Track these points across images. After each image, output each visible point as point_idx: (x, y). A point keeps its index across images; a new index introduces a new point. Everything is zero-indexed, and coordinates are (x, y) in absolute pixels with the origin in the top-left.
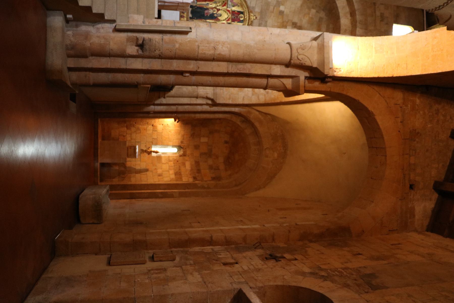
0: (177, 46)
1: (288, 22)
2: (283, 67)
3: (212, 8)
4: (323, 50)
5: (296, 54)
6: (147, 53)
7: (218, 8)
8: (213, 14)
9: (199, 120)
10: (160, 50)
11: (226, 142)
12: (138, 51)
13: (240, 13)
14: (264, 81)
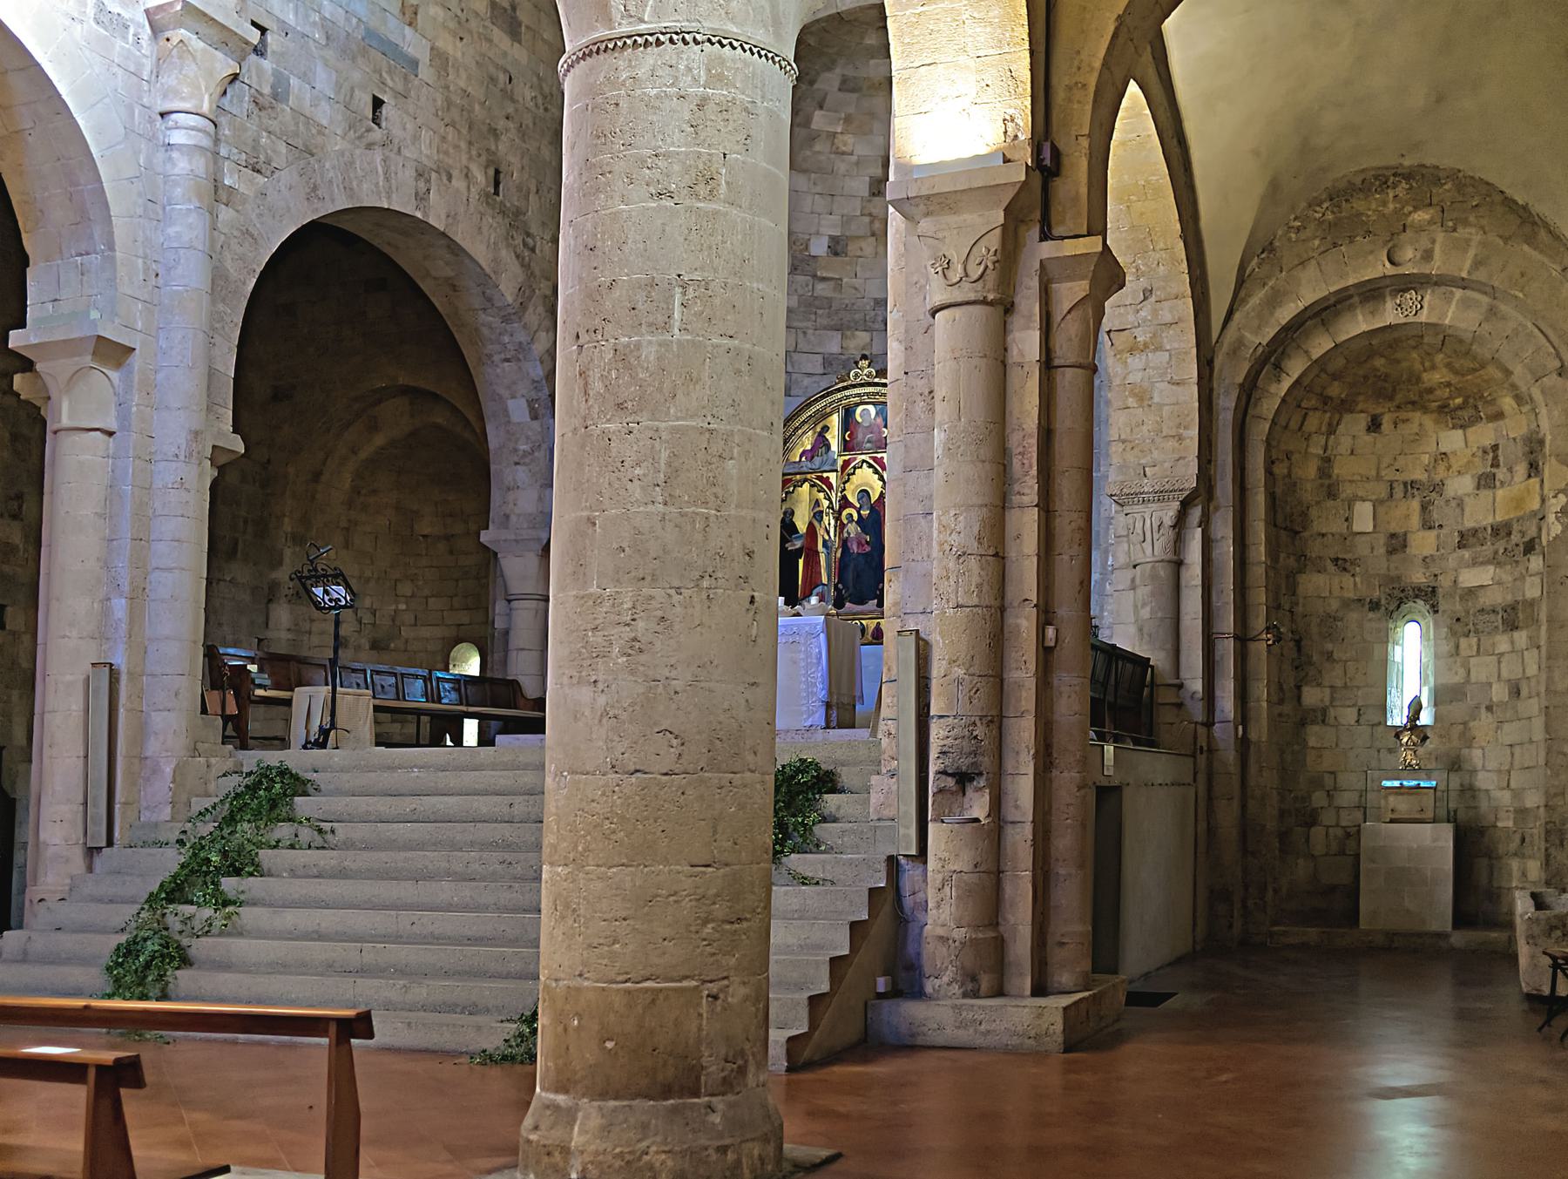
0: (960, 672)
1: (870, 215)
2: (1016, 321)
3: (841, 527)
4: (939, 197)
5: (966, 285)
6: (986, 762)
7: (836, 507)
8: (861, 521)
9: (1273, 550)
10: (974, 724)
11: (1375, 425)
12: (979, 789)
13: (848, 422)
14: (1068, 380)
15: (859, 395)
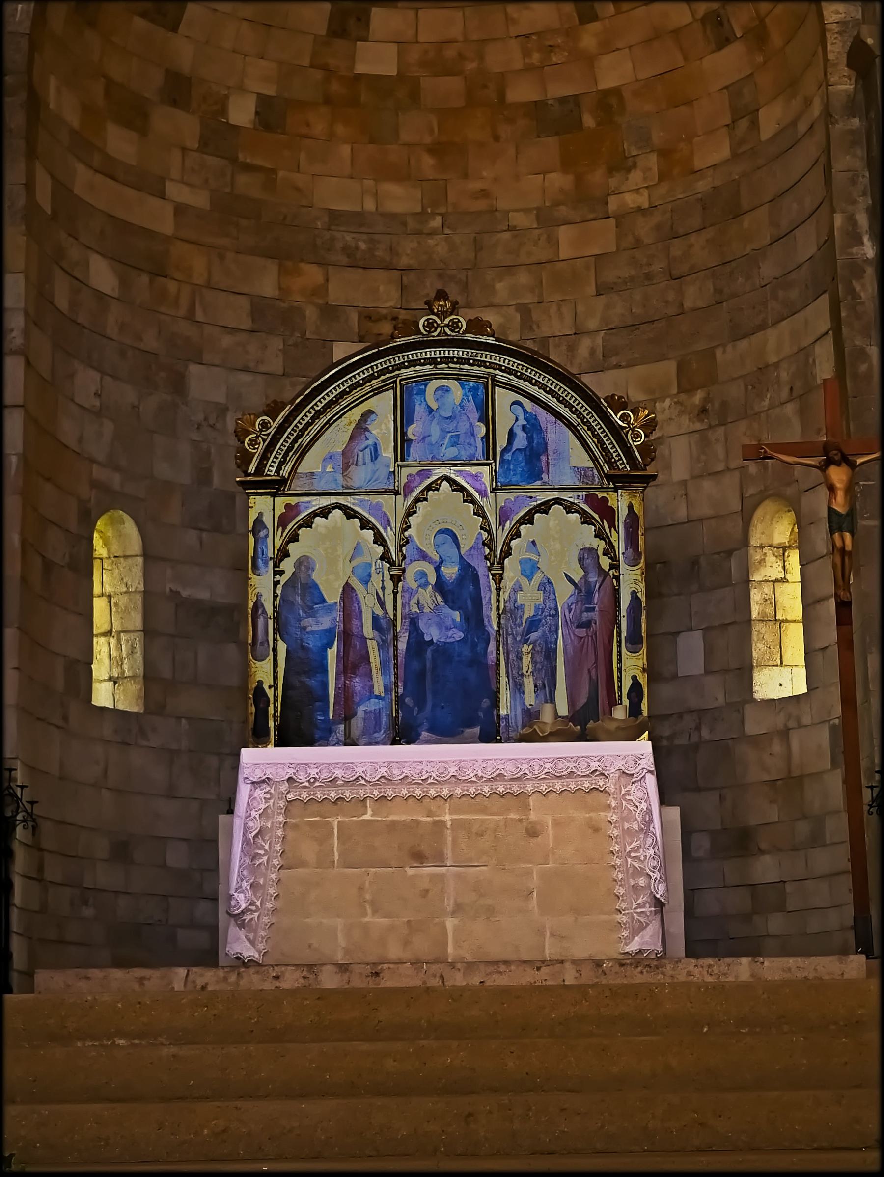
15: (433, 361)
